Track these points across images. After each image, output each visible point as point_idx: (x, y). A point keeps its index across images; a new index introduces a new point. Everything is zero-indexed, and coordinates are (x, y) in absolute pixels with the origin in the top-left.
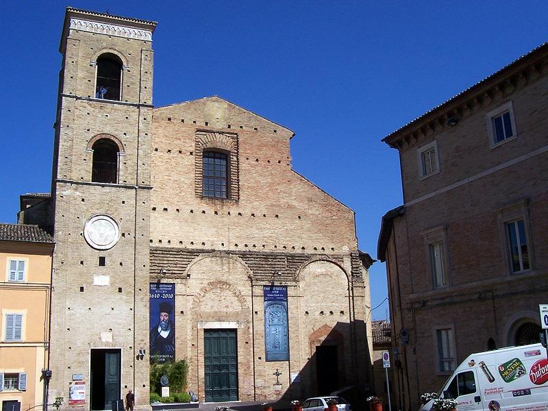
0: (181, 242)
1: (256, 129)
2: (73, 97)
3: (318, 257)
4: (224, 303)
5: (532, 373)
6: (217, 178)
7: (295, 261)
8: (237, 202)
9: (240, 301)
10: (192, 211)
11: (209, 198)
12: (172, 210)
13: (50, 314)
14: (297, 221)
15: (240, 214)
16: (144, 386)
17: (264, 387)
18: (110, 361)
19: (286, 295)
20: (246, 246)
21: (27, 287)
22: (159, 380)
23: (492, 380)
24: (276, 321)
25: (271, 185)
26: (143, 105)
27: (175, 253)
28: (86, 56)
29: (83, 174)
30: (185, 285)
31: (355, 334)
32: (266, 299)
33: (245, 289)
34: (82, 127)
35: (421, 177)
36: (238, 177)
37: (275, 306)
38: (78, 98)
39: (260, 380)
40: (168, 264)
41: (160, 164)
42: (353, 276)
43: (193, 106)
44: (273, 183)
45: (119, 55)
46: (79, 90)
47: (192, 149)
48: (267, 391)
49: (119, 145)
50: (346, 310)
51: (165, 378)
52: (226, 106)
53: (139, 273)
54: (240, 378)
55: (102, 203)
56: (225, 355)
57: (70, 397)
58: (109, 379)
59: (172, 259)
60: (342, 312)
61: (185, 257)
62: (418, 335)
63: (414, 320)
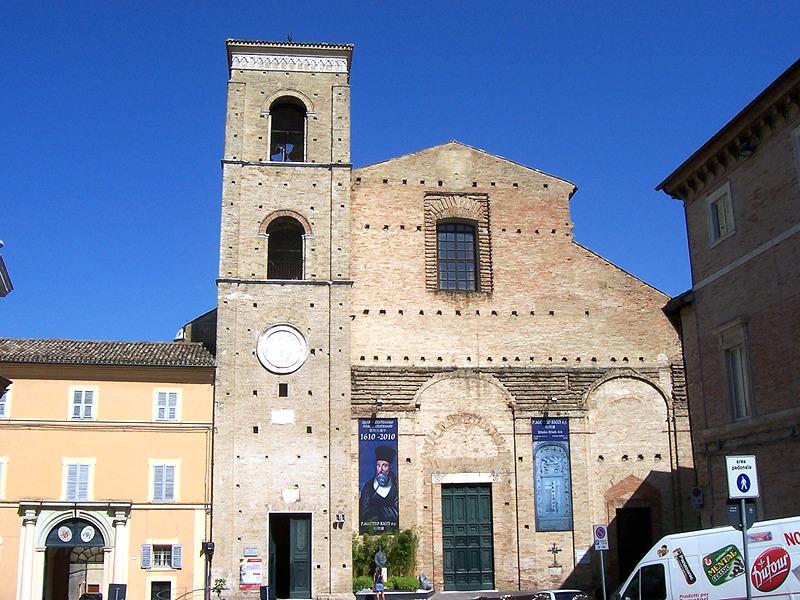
0: (406, 358)
1: (515, 185)
2: (238, 163)
3: (618, 373)
4: (472, 445)
5: (756, 572)
6: (461, 261)
7: (582, 379)
8: (489, 295)
9: (495, 442)
10: (422, 313)
11: (447, 291)
12: (392, 312)
13: (213, 464)
14: (584, 319)
15: (494, 313)
16: (344, 566)
17: (534, 571)
18: (296, 530)
19: (566, 431)
20: (505, 359)
21: (181, 428)
22: (373, 558)
23: (691, 580)
24: (551, 470)
25: (540, 267)
26: (336, 165)
27: (397, 374)
28: (256, 104)
29: (255, 268)
30: (413, 419)
31: (679, 489)
32: (536, 437)
33: (504, 424)
34: (252, 203)
35: (713, 242)
36: (490, 259)
37: (550, 448)
38: (244, 164)
39: (527, 560)
40: (386, 391)
41: (373, 246)
42: (675, 399)
43: (419, 159)
44: (545, 264)
45: (301, 97)
46: (246, 153)
47: (420, 222)
48: (538, 577)
49: (304, 224)
50: (665, 453)
51: (382, 556)
52: (468, 154)
53: (336, 405)
54: (497, 557)
55: (281, 307)
56: (475, 522)
57: (241, 580)
58: (294, 556)
59: (393, 383)
60: (658, 456)
61: (413, 379)
62: (716, 495)
63: (710, 471)
